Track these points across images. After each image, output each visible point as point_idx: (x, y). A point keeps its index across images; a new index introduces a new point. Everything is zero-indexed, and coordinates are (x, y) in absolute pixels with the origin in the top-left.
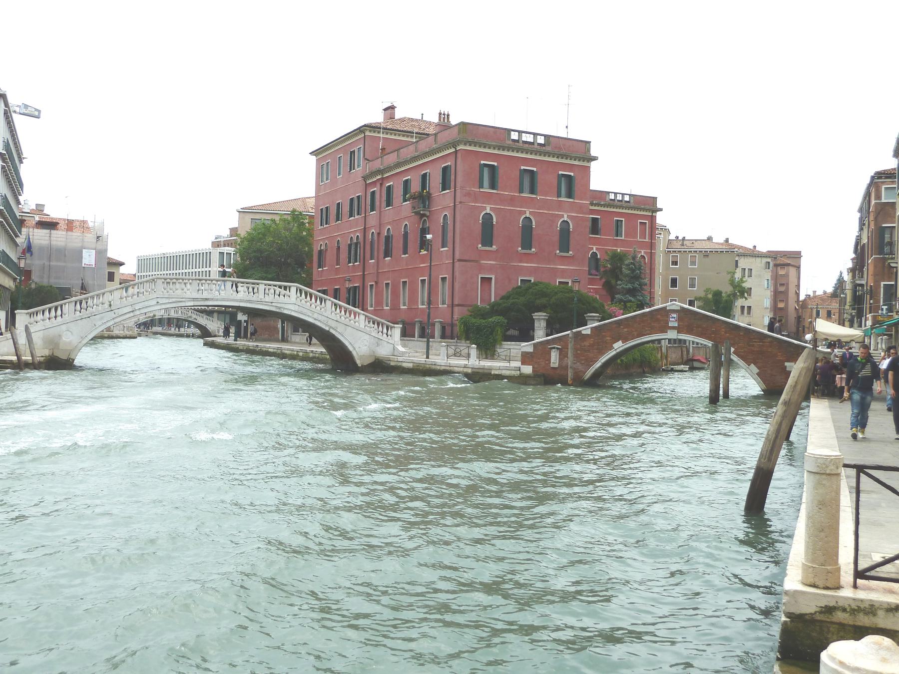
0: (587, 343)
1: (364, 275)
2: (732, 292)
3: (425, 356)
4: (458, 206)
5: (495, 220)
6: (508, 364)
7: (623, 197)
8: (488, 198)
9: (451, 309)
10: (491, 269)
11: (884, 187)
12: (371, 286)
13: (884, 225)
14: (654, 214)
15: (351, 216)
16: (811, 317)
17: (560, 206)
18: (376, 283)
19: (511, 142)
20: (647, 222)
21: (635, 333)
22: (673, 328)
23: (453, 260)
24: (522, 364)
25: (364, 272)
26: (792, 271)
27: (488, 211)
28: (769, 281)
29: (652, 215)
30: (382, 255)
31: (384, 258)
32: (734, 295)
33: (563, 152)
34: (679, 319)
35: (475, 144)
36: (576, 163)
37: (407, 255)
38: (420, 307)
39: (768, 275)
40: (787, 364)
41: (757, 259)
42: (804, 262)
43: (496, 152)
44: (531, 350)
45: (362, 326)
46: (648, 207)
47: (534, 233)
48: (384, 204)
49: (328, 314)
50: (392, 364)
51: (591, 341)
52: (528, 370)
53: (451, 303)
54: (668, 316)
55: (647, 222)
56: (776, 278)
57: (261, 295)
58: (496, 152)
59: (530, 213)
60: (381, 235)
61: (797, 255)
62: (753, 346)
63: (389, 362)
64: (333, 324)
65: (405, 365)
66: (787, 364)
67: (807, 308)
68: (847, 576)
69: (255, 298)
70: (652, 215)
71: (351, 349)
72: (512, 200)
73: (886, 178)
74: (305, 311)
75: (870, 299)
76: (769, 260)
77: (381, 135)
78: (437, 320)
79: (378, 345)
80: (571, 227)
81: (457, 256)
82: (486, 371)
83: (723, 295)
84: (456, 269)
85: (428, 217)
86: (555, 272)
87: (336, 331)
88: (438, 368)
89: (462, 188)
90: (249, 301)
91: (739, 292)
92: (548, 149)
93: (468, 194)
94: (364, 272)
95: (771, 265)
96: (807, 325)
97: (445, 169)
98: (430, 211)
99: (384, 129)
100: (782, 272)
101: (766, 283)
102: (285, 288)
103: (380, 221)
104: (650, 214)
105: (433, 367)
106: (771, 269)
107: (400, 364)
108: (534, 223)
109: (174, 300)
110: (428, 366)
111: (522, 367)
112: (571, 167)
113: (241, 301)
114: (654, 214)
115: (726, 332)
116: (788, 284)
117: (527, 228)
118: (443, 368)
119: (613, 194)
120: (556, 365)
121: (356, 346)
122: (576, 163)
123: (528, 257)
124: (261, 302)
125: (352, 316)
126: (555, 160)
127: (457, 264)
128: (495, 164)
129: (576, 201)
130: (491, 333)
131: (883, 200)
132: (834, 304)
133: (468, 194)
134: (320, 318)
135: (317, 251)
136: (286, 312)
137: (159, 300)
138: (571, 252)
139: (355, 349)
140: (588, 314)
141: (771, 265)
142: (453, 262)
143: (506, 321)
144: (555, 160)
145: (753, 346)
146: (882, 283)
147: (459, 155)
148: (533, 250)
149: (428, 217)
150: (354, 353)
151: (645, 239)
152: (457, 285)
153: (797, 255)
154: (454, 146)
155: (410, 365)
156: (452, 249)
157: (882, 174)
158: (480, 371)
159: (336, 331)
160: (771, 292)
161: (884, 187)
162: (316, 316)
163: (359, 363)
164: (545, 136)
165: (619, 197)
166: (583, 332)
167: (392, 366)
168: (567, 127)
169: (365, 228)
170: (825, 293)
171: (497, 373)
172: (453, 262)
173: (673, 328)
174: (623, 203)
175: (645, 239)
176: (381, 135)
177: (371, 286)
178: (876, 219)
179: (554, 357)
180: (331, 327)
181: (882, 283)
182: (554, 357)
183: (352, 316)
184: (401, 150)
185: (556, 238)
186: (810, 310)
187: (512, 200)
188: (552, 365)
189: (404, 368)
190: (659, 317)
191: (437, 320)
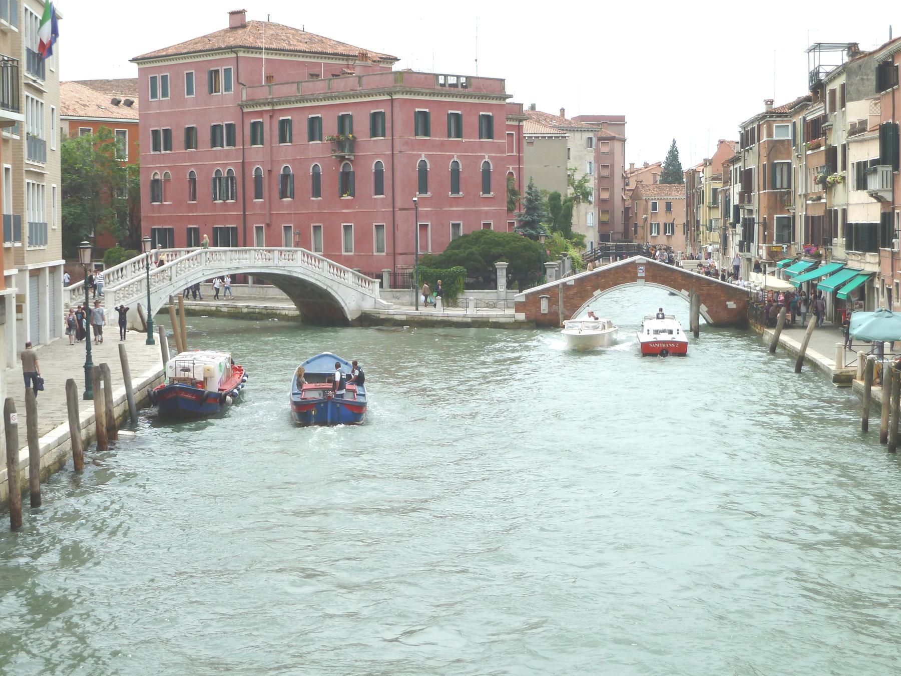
0: (571, 292)
1: (245, 215)
2: (573, 194)
3: (415, 308)
4: (398, 156)
5: (428, 166)
6: (503, 313)
7: (445, 80)
8: (423, 145)
9: (392, 258)
10: (427, 215)
11: (775, 125)
12: (259, 229)
13: (776, 162)
14: (521, 124)
15: (214, 144)
16: (646, 211)
17: (481, 147)
18: (268, 225)
19: (439, 87)
20: (514, 132)
21: (611, 283)
22: (641, 278)
23: (394, 208)
24: (516, 312)
25: (244, 211)
26: (617, 145)
27: (423, 158)
28: (593, 164)
29: (519, 126)
30: (276, 194)
31: (281, 198)
32: (576, 198)
33: (484, 93)
34: (646, 271)
35: (411, 93)
36: (494, 102)
37: (319, 198)
38: (344, 253)
39: (590, 156)
40: (728, 303)
41: (576, 134)
42: (629, 131)
43: (428, 98)
44: (523, 299)
45: (351, 283)
46: (514, 117)
47: (461, 176)
48: (276, 138)
49: (325, 273)
50: (382, 317)
51: (575, 290)
52: (521, 316)
53: (391, 251)
54: (636, 268)
55: (514, 132)
56: (599, 156)
57: (276, 262)
58: (428, 98)
59: (458, 156)
60: (273, 173)
61: (619, 122)
62: (703, 290)
63: (378, 315)
64: (329, 283)
65: (396, 317)
66: (728, 303)
67: (641, 199)
68: (843, 367)
69: (270, 263)
70: (519, 126)
71: (343, 304)
72: (442, 146)
73: (777, 117)
74: (308, 273)
75: (765, 231)
76: (591, 135)
77: (264, 56)
78: (386, 270)
79: (363, 300)
80: (491, 167)
81: (399, 204)
82: (484, 320)
83: (562, 198)
84: (397, 218)
85: (352, 161)
86: (478, 214)
87: (332, 289)
88: (435, 318)
89: (401, 137)
90: (268, 267)
91: (582, 194)
92: (470, 90)
93: (406, 143)
94: (244, 211)
95: (594, 140)
96: (640, 223)
97: (374, 116)
98: (354, 156)
99: (266, 49)
100: (605, 149)
101: (588, 167)
102: (269, 251)
103: (271, 157)
104: (517, 123)
105: (430, 318)
106: (594, 147)
107: (390, 317)
108: (461, 167)
109: (215, 271)
110: (423, 317)
111: (516, 314)
112: (489, 107)
113: (263, 267)
114: (521, 124)
115: (682, 280)
116: (613, 166)
117: (455, 173)
118: (439, 319)
119: (443, 77)
120: (546, 312)
121: (347, 302)
122: (494, 102)
123: (456, 201)
124: (276, 267)
125: (342, 273)
126: (476, 101)
127: (399, 214)
128: (427, 110)
129: (495, 141)
130: (453, 283)
131: (775, 138)
132: (673, 193)
133: (406, 143)
134: (320, 278)
135: (149, 184)
136: (295, 275)
137: (204, 272)
138: (492, 193)
139: (346, 304)
140: (547, 263)
141: (594, 140)
142: (394, 211)
143: (465, 270)
144: (476, 101)
145: (703, 290)
146: (775, 216)
147: (396, 104)
148: (461, 193)
149: (352, 161)
150: (346, 308)
151: (512, 152)
152: (399, 234)
153: (619, 122)
154: (390, 94)
155: (404, 318)
156: (391, 195)
157: (773, 113)
158: (479, 320)
159: (332, 289)
160: (595, 179)
161: (775, 125)
162: (316, 276)
163: (350, 317)
164: (467, 78)
165: (452, 80)
166: (568, 283)
167: (382, 319)
168: (476, 60)
169: (243, 162)
170: (646, 165)
171: (494, 320)
172: (394, 211)
173: (641, 278)
174: (447, 88)
175: (512, 152)
176: (264, 56)
177: (259, 229)
178: (768, 155)
179: (544, 306)
180: (328, 286)
181: (775, 216)
182: (544, 306)
183: (342, 273)
184: (303, 84)
185: (479, 180)
186: (644, 202)
187: (442, 146)
188: (543, 312)
189: (396, 321)
190: (630, 269)
191: (386, 270)
